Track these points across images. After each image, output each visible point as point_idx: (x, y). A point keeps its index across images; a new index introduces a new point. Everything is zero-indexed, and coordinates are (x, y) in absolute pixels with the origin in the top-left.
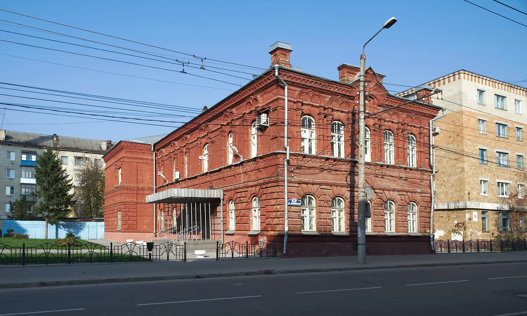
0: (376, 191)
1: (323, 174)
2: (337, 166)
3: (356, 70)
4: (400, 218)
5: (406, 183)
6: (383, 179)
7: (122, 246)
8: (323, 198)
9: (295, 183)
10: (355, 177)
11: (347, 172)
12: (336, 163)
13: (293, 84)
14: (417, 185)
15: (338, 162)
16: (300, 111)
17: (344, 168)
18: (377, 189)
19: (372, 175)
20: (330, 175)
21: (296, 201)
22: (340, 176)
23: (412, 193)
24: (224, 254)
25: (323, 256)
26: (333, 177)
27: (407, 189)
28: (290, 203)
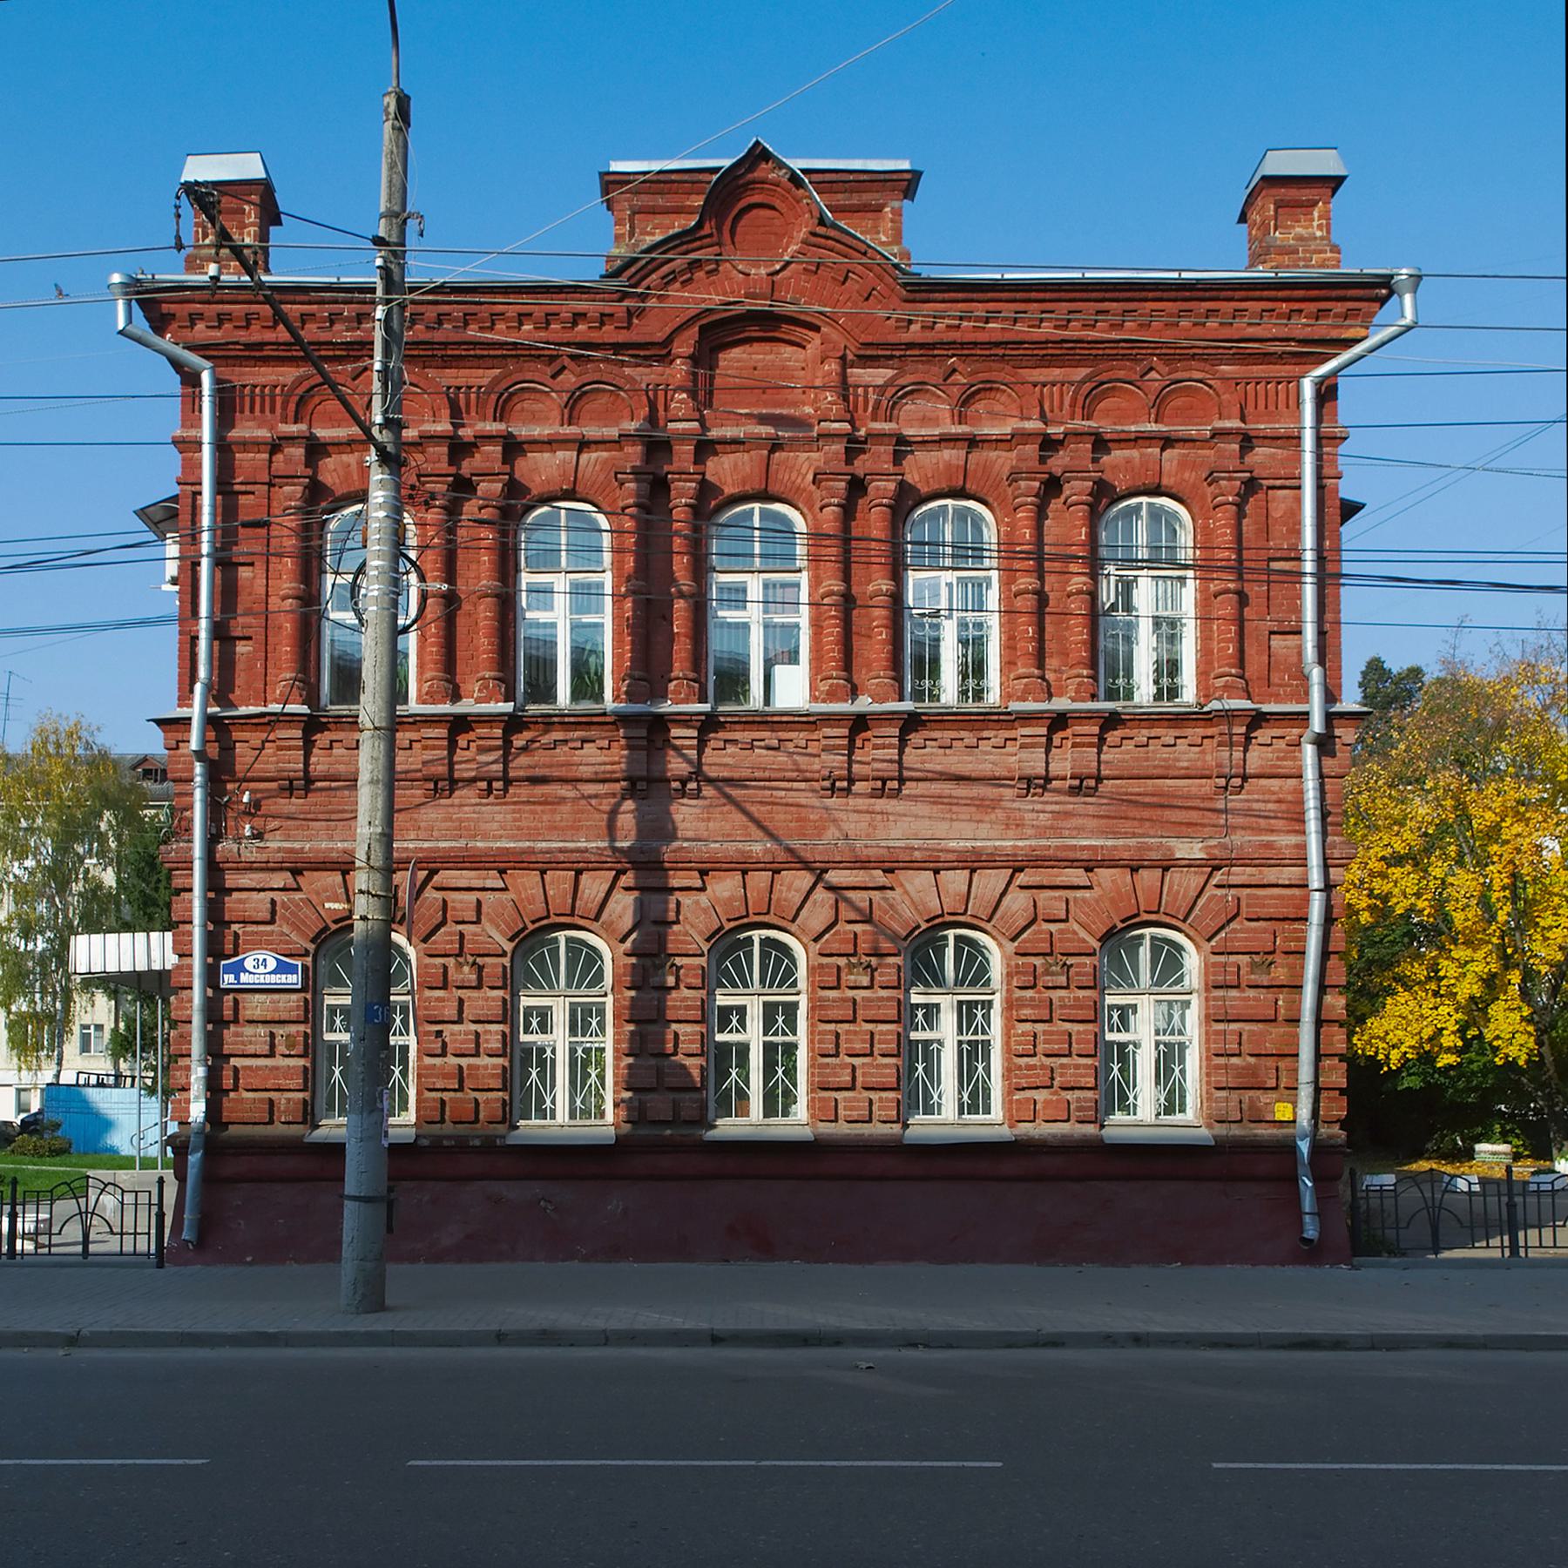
0: (833, 877)
1: (450, 810)
2: (540, 757)
3: (693, 183)
4: (1023, 1034)
5: (1080, 809)
6: (894, 802)
7: (51, 1191)
8: (448, 942)
9: (266, 867)
10: (673, 808)
11: (617, 781)
12: (533, 741)
13: (257, 354)
14: (1177, 812)
15: (546, 732)
16: (294, 485)
17: (593, 760)
18: (838, 865)
19: (803, 785)
20: (498, 808)
21: (272, 964)
22: (566, 808)
23: (1134, 870)
24: (128, 1240)
25: (438, 1257)
26: (515, 820)
27: (1083, 848)
28: (237, 978)
